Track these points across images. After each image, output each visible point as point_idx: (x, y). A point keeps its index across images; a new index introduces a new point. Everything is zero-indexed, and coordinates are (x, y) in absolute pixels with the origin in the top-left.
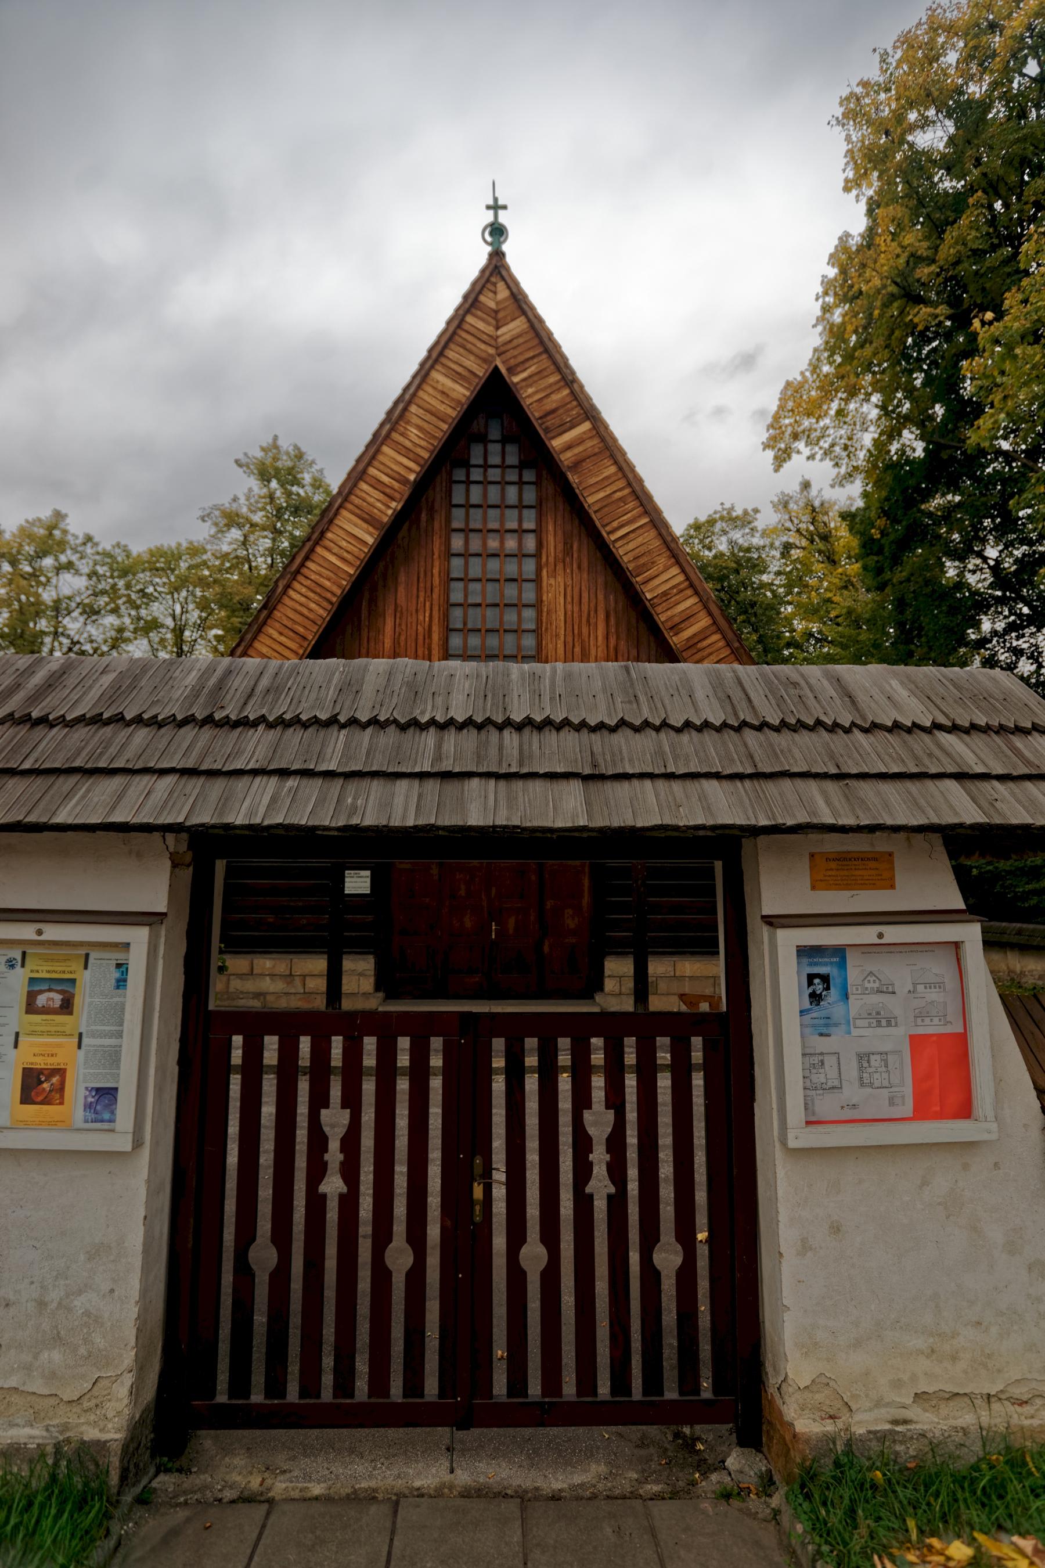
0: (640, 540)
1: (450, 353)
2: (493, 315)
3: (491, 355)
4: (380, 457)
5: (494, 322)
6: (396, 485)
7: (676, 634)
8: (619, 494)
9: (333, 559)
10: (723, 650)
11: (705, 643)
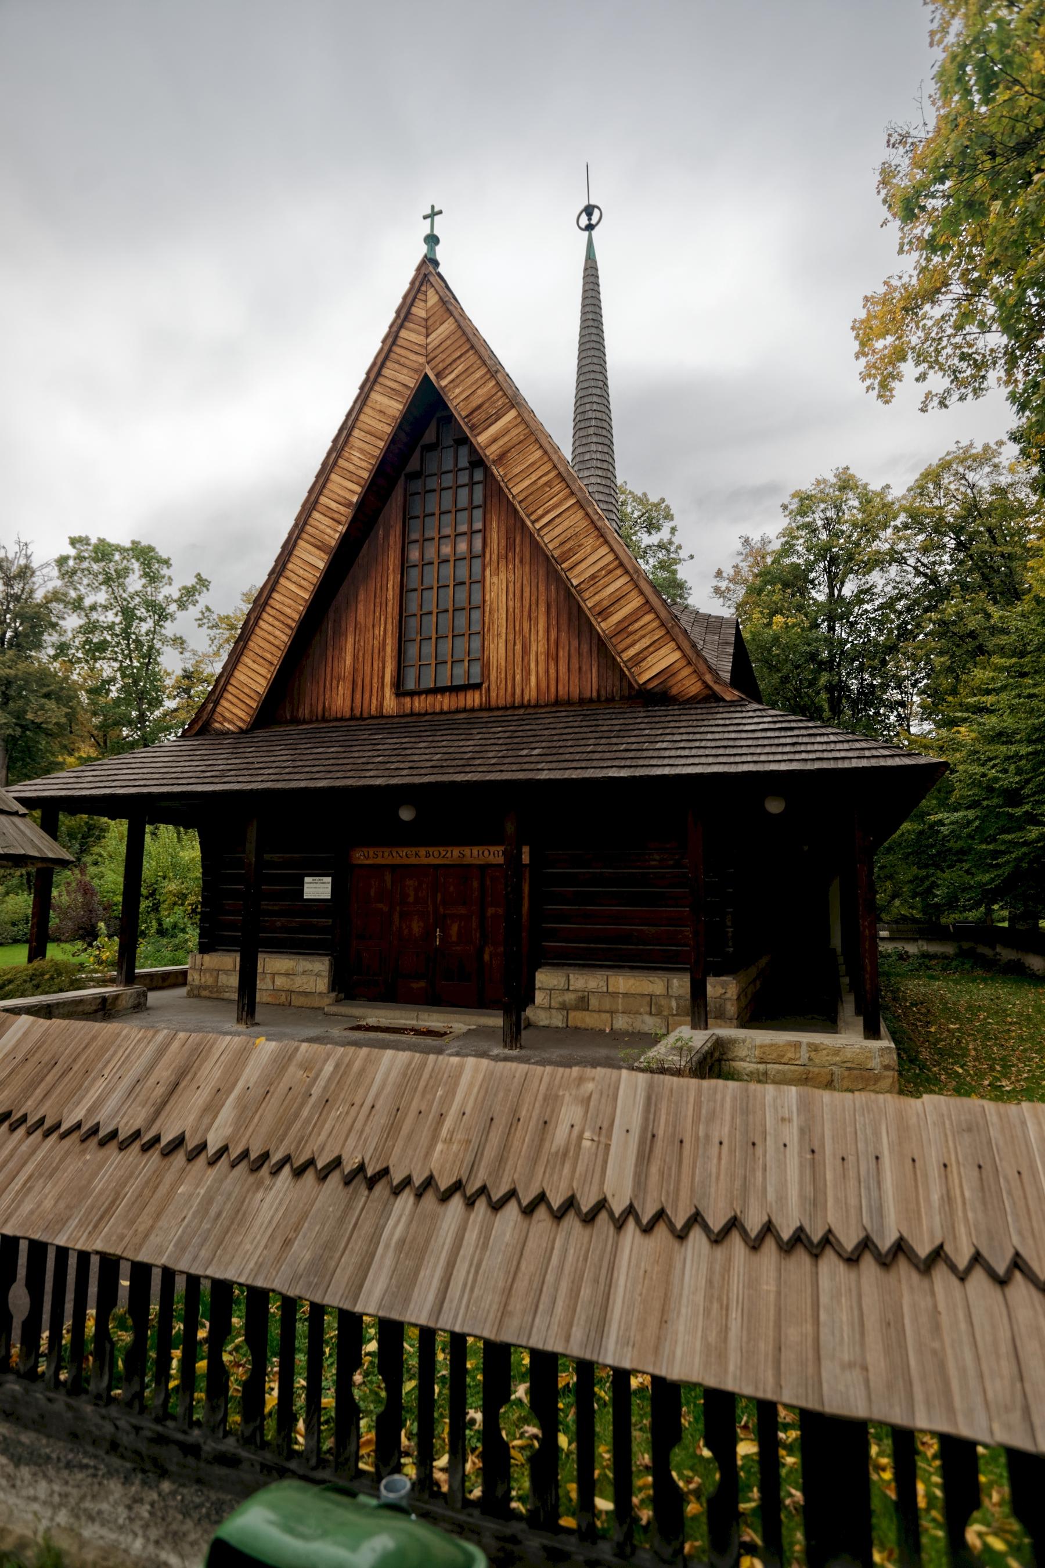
0: (566, 524)
1: (386, 372)
3: (421, 364)
4: (329, 485)
5: (424, 330)
6: (342, 509)
7: (604, 620)
8: (545, 479)
9: (293, 587)
11: (637, 626)
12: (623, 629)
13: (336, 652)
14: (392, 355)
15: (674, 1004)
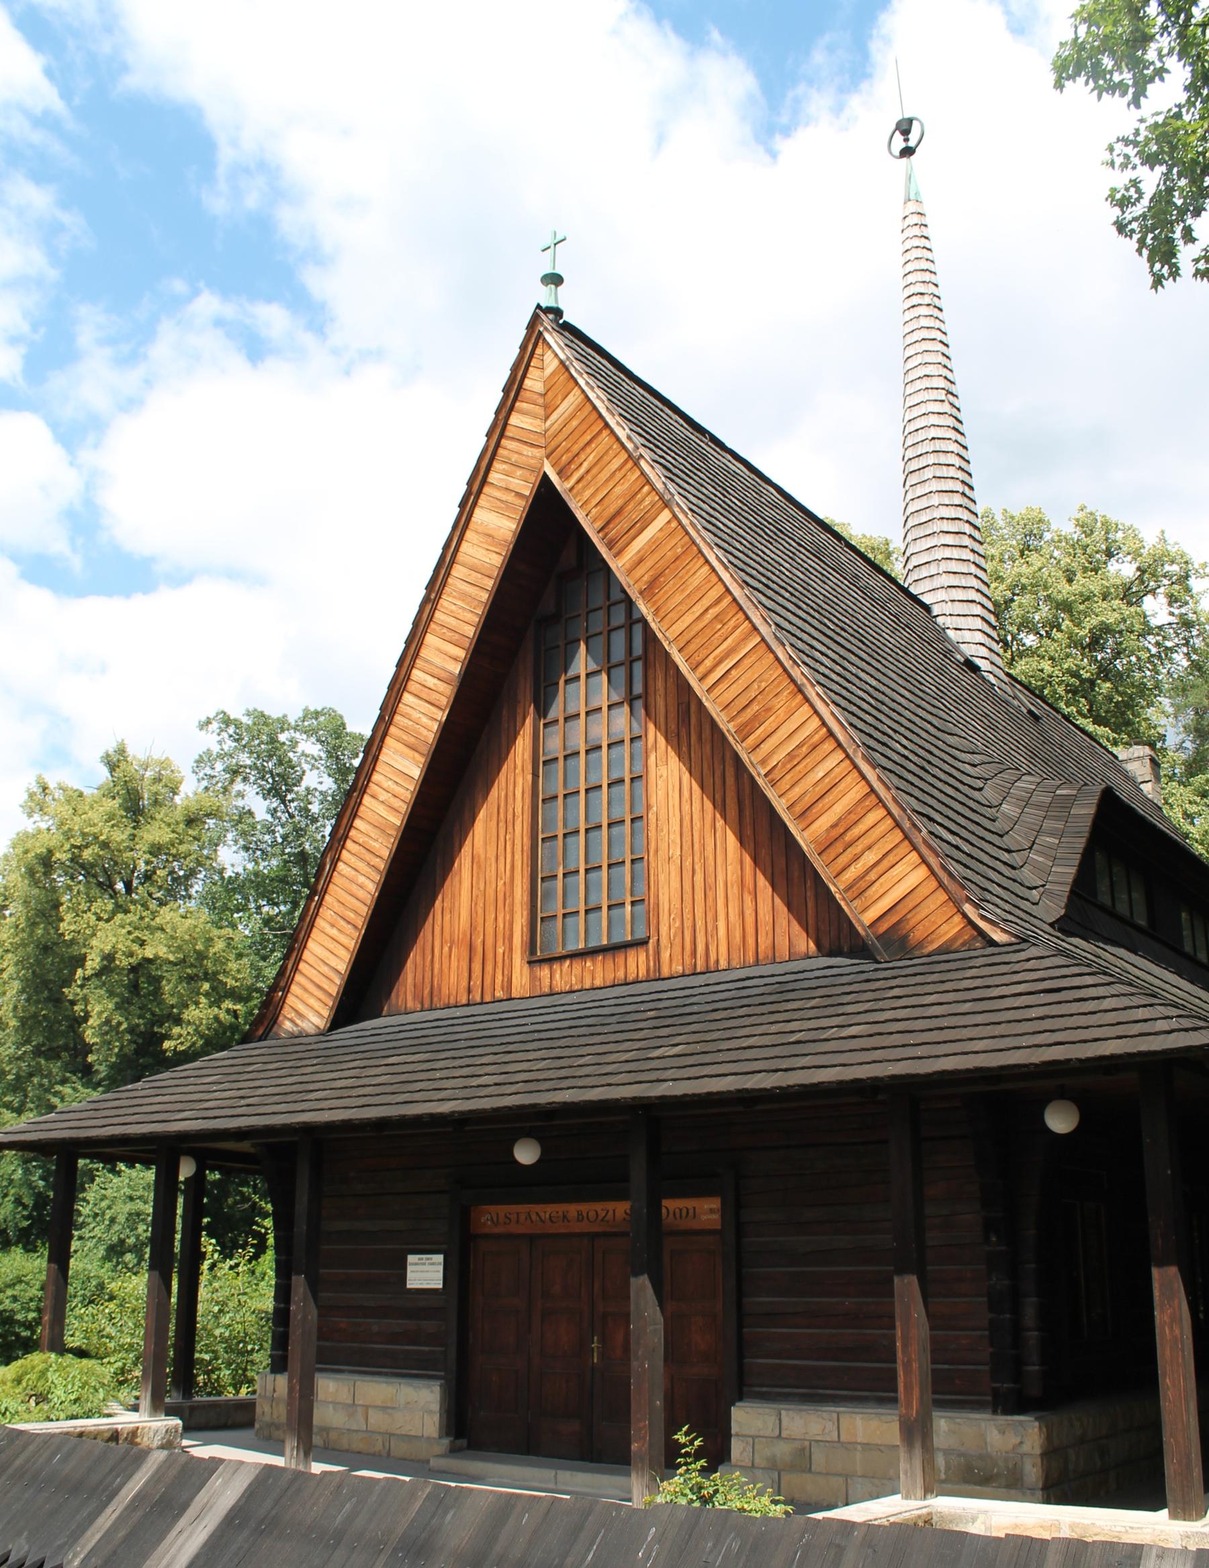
1: (494, 477)
2: (541, 401)
8: (712, 612)
10: (889, 837)
11: (856, 831)
12: (832, 842)
14: (501, 451)
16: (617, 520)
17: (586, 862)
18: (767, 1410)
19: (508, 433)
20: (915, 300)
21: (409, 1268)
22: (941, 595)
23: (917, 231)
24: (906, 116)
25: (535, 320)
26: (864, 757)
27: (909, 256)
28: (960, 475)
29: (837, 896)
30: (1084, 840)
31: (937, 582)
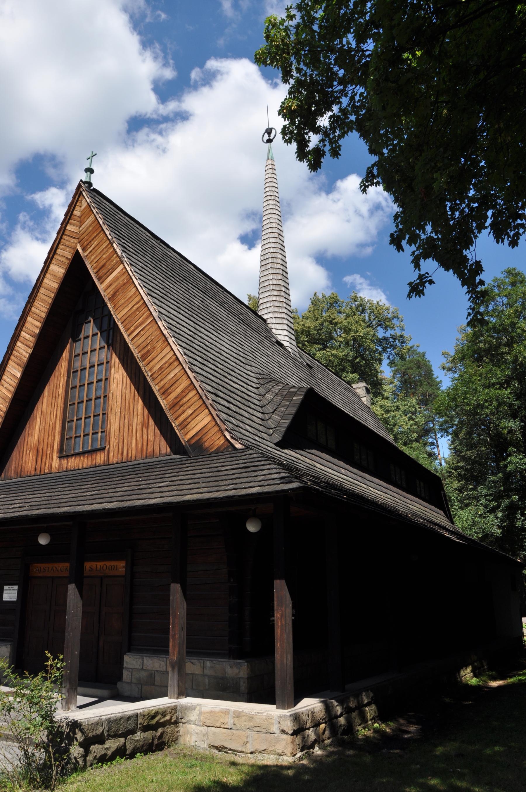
1: (59, 251)
2: (79, 219)
10: (197, 403)
11: (185, 400)
13: (30, 432)
14: (62, 240)
15: (207, 680)
16: (103, 268)
17: (85, 414)
18: (138, 657)
19: (66, 233)
20: (269, 198)
21: (5, 592)
22: (271, 315)
23: (270, 171)
24: (270, 127)
25: (79, 186)
26: (189, 368)
27: (267, 181)
28: (282, 267)
29: (175, 428)
30: (296, 409)
31: (270, 310)
